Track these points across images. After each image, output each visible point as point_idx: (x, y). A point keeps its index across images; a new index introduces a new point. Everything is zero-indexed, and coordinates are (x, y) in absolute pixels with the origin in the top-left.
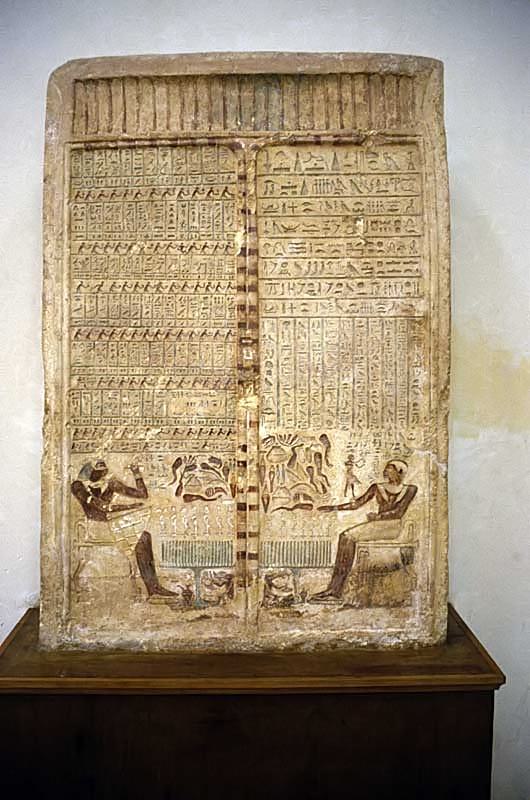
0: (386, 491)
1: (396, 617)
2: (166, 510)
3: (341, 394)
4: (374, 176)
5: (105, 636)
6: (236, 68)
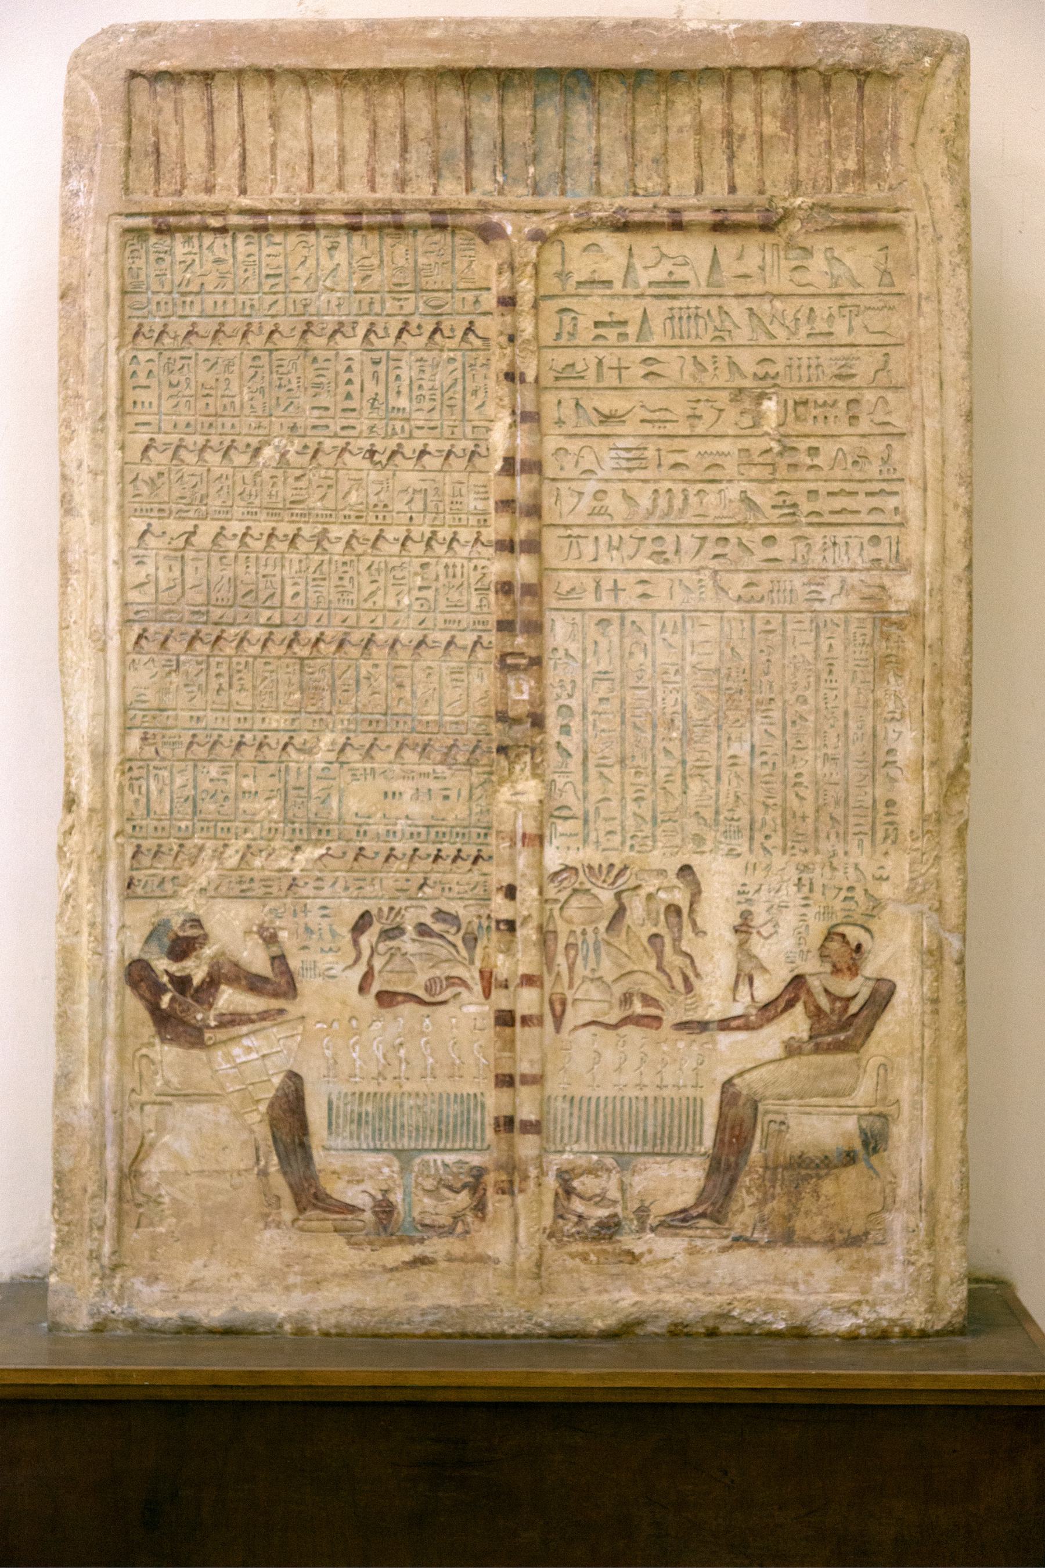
0: (826, 991)
1: (852, 1268)
2: (336, 1025)
3: (725, 778)
4: (802, 301)
5: (196, 1303)
6: (494, 52)
